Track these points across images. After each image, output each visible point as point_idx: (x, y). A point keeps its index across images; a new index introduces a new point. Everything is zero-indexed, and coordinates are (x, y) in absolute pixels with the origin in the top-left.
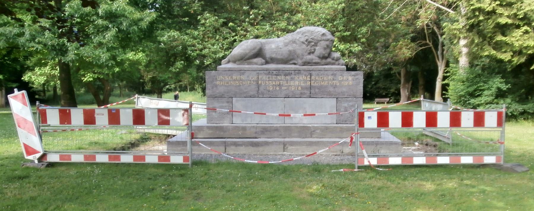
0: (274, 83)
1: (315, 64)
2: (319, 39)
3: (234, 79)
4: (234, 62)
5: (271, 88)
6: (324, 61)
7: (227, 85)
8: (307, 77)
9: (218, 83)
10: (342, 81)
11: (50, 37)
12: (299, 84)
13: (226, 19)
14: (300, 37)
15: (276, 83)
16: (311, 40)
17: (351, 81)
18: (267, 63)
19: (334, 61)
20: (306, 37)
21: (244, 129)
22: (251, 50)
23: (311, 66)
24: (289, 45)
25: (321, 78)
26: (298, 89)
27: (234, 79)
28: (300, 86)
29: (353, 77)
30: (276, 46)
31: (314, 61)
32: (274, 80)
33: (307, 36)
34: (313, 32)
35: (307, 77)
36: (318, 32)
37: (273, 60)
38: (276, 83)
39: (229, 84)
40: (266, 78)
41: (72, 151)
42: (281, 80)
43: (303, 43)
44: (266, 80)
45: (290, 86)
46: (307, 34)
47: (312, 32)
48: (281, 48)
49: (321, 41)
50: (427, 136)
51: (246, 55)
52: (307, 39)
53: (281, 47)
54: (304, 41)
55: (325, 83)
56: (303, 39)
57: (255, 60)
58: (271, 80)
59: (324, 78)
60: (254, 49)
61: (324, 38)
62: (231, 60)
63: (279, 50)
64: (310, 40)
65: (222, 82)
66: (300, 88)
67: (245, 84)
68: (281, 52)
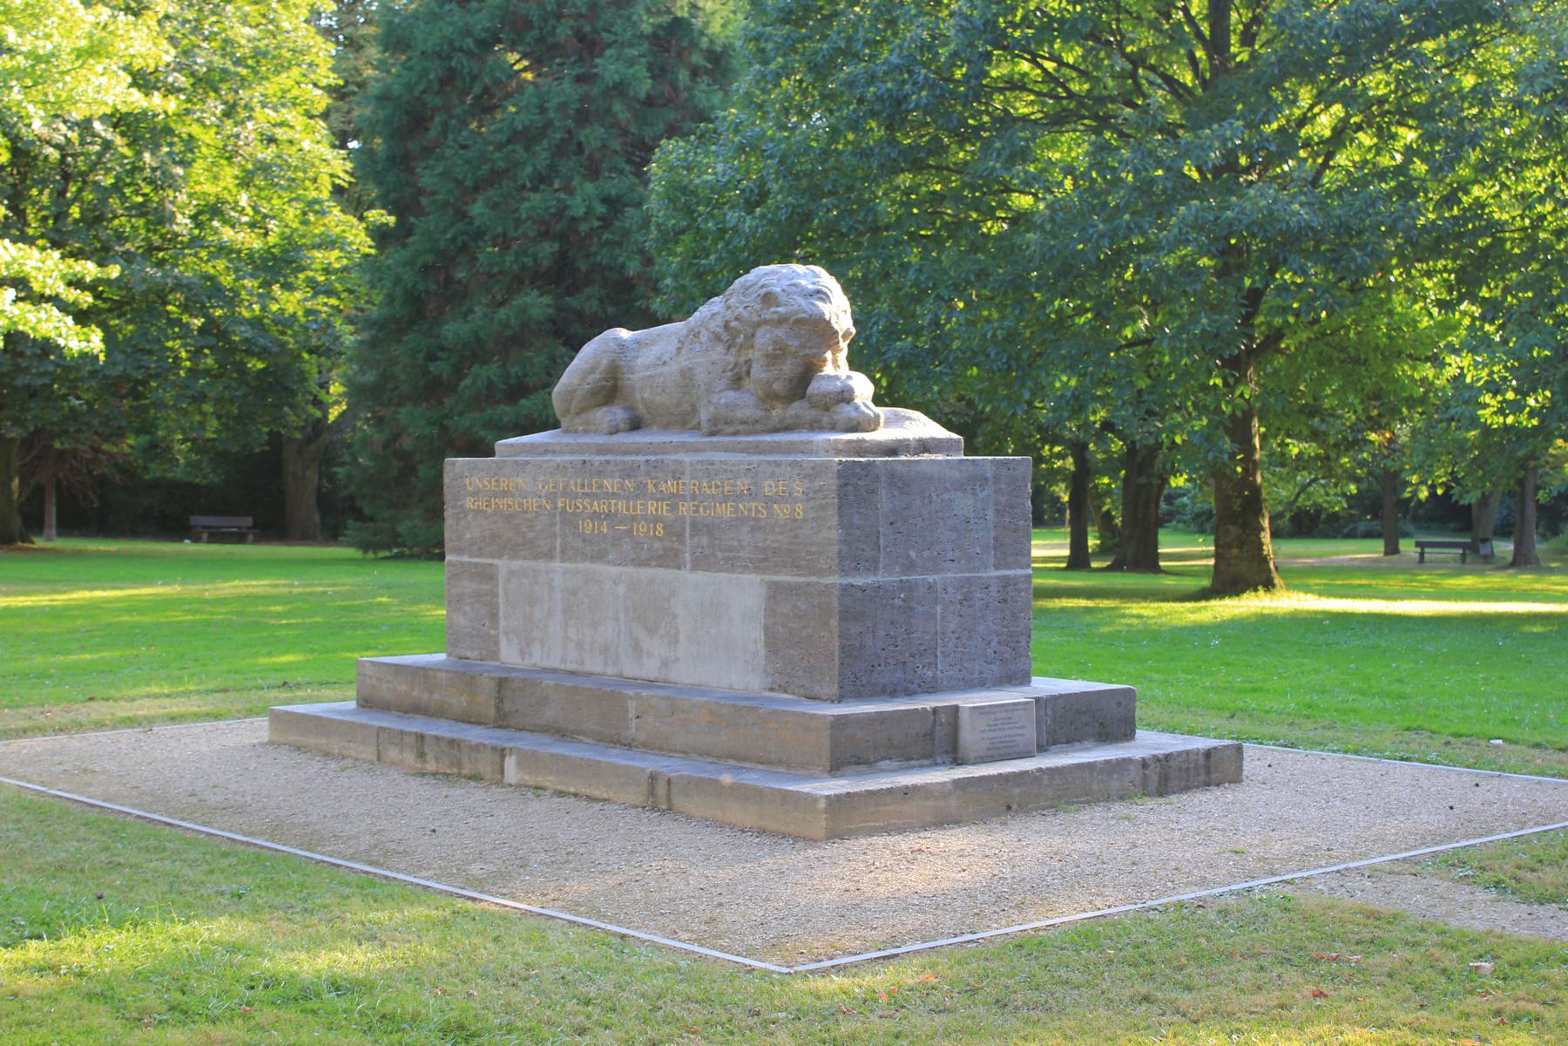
31: (739, 414)
60: (592, 370)
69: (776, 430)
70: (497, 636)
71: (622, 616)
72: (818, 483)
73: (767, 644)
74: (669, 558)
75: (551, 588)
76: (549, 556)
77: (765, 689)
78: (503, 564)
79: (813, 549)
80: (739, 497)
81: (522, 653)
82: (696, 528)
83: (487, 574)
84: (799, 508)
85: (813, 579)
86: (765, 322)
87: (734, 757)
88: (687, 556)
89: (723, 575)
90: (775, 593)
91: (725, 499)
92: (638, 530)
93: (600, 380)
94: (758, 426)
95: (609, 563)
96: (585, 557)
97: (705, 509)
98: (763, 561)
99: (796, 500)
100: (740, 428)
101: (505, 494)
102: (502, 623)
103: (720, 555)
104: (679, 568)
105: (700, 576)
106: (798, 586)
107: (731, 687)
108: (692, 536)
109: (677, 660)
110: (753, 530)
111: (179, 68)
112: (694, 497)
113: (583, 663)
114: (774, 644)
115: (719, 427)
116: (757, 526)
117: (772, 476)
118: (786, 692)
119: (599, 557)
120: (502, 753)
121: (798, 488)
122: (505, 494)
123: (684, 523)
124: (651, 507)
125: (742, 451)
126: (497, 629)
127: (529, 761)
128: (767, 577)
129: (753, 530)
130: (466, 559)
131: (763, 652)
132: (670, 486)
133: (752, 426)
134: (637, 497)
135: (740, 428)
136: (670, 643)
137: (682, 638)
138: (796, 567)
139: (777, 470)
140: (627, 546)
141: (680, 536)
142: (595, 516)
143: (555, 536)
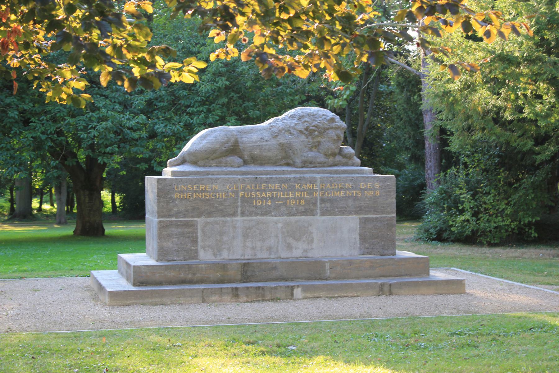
0: (264, 194)
1: (320, 165)
2: (326, 126)
3: (202, 189)
4: (195, 163)
5: (259, 202)
6: (331, 159)
7: (191, 198)
8: (313, 185)
9: (176, 196)
10: (365, 190)
11: (424, 208)
12: (301, 195)
13: (472, 191)
14: (296, 124)
15: (266, 194)
16: (314, 128)
17: (379, 190)
18: (245, 163)
19: (345, 160)
20: (306, 123)
21: (223, 266)
22: (223, 144)
23: (314, 167)
24: (279, 136)
25: (335, 186)
26: (300, 202)
27: (202, 189)
28: (304, 198)
29: (381, 184)
30: (260, 137)
31: (318, 160)
32: (265, 191)
33: (307, 122)
34: (316, 115)
35: (313, 185)
36: (323, 115)
37: (255, 160)
38: (266, 194)
39: (194, 197)
40: (251, 187)
41: (202, 287)
42: (275, 190)
43: (301, 132)
44: (251, 191)
45: (287, 198)
46: (306, 119)
47: (313, 116)
48: (267, 141)
49: (328, 129)
50: (51, 333)
51: (214, 151)
52: (307, 127)
53: (267, 138)
54: (303, 130)
55: (340, 193)
56: (301, 127)
57: (229, 159)
58: (258, 190)
59: (338, 186)
60: (227, 142)
61: (334, 125)
62: (188, 159)
63: (265, 143)
64: (311, 128)
65: (184, 194)
66: (303, 202)
67: (219, 197)
68: (267, 147)
69: (331, 166)
70: (197, 250)
71: (280, 236)
72: (386, 184)
73: (360, 239)
74: (312, 213)
75: (234, 227)
76: (234, 214)
77: (360, 255)
78: (200, 221)
79: (384, 205)
80: (348, 189)
81: (215, 255)
82: (323, 201)
83: (192, 225)
84: (378, 193)
85: (384, 215)
86: (332, 128)
87: (384, 276)
88: (318, 211)
89: (337, 217)
90: (364, 222)
91: (340, 190)
92: (290, 203)
93: (232, 146)
94: (325, 165)
95: (272, 216)
96: (257, 214)
97: (328, 194)
98: (358, 211)
99: (376, 189)
100: (317, 165)
101: (203, 191)
102: (200, 243)
103: (336, 210)
104: (314, 216)
105: (325, 218)
106: (377, 218)
107: (342, 256)
108: (321, 204)
109: (312, 249)
110: (354, 200)
111: (451, 48)
112: (322, 190)
113: (255, 255)
114: (363, 238)
115: (306, 165)
116: (356, 198)
117: (364, 182)
118: (370, 254)
119: (267, 213)
120: (292, 288)
121: (377, 185)
122: (203, 191)
123: (317, 199)
124: (298, 194)
125: (327, 173)
126: (197, 246)
127: (306, 289)
128: (361, 216)
129: (354, 200)
130: (174, 219)
131: (358, 242)
132: (309, 186)
133: (323, 164)
134: (289, 191)
135: (317, 165)
136: (308, 243)
137: (315, 241)
138: (376, 211)
139: (367, 180)
140: (283, 209)
141: (315, 204)
142: (262, 199)
143: (237, 207)
